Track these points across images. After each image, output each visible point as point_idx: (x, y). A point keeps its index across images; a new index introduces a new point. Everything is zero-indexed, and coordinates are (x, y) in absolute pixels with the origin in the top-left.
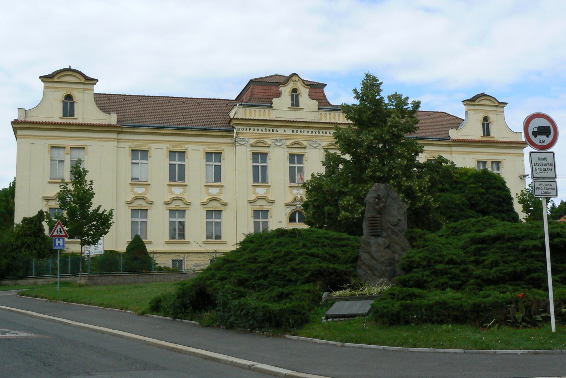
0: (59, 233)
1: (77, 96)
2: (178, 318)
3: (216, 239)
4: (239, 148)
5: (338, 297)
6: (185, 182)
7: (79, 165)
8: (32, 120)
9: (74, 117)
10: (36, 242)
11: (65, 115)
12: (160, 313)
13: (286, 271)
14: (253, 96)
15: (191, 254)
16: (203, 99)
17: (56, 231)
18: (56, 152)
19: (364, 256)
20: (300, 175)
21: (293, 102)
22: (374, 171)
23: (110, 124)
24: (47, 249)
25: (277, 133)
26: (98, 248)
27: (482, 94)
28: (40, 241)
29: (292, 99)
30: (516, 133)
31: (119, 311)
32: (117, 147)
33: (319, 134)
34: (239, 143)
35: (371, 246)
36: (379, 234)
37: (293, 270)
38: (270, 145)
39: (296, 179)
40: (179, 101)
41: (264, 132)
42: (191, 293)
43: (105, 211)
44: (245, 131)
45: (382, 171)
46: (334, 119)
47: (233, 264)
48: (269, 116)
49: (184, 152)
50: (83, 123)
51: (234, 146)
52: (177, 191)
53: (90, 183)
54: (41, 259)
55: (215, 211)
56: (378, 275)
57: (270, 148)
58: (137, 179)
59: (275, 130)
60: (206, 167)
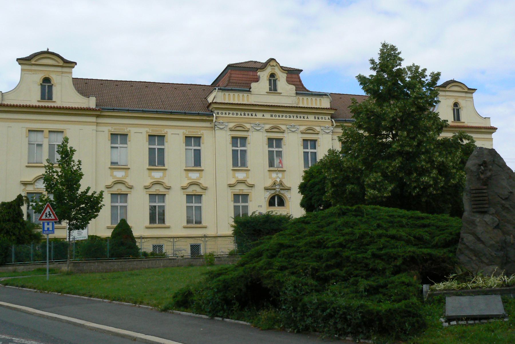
0: (48, 216)
1: (55, 78)
2: (217, 316)
3: (196, 223)
4: (218, 133)
5: (224, 271)
6: (164, 166)
7: (66, 143)
8: (9, 103)
9: (52, 100)
10: (15, 227)
11: (43, 98)
12: (189, 309)
13: (367, 258)
14: (231, 80)
15: (180, 239)
16: (180, 84)
17: (45, 214)
18: (33, 135)
19: (468, 238)
20: (279, 159)
21: (271, 87)
22: (402, 146)
23: (89, 108)
24: (26, 234)
25: (256, 117)
26: (82, 233)
27: (451, 80)
28: (19, 226)
29: (270, 84)
30: (485, 118)
31: (132, 306)
32: (96, 131)
33: (297, 119)
34: (218, 127)
35: (476, 225)
36: (486, 210)
37: (374, 255)
38: (249, 129)
39: (275, 163)
40: (156, 86)
41: (243, 116)
42: (237, 286)
43: (95, 192)
44: (224, 115)
45: (410, 146)
46: (312, 103)
47: (292, 250)
48: (248, 100)
49: (163, 136)
50: (62, 106)
51: (214, 131)
52: (157, 175)
53: (78, 163)
54: (20, 245)
55: (195, 195)
56: (486, 261)
57: (284, 134)
58: (116, 163)
59: (254, 115)
60: (186, 151)
